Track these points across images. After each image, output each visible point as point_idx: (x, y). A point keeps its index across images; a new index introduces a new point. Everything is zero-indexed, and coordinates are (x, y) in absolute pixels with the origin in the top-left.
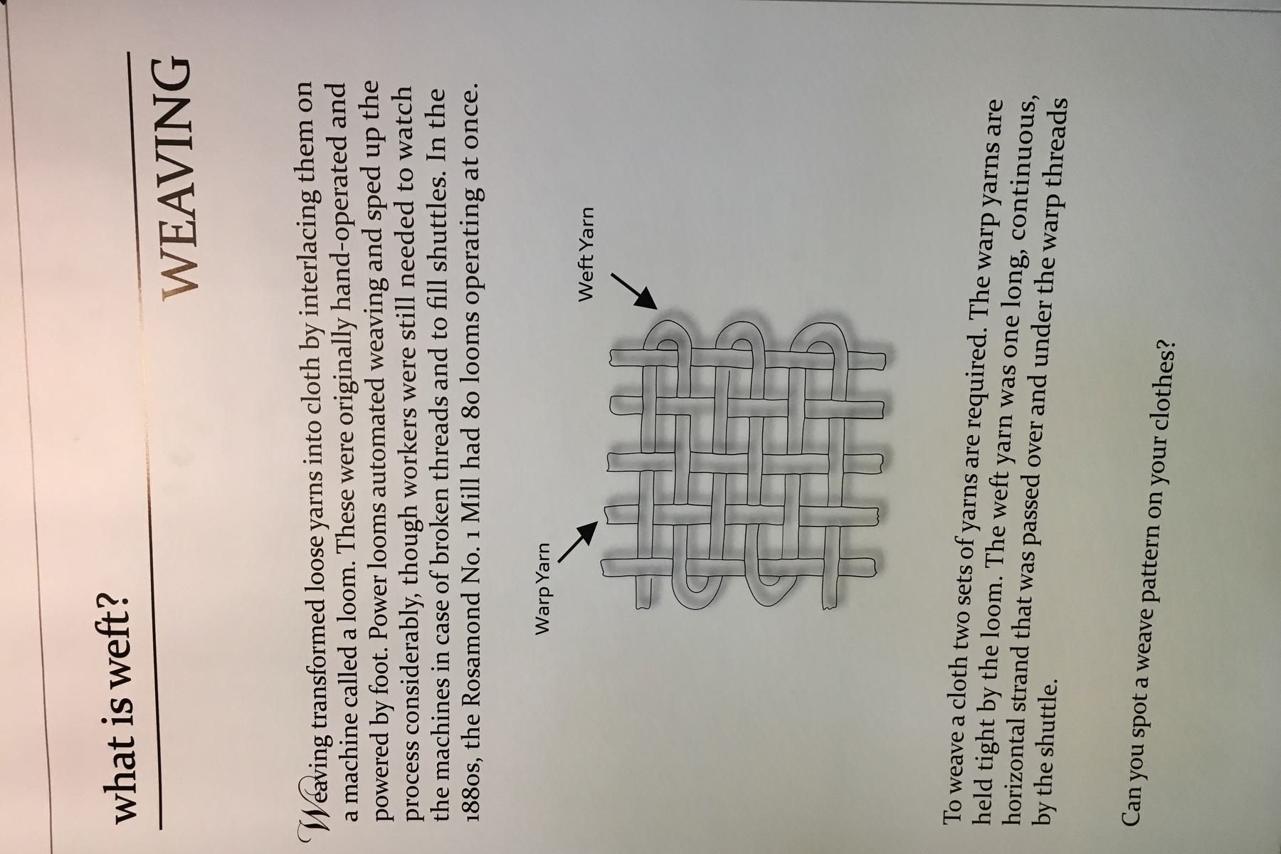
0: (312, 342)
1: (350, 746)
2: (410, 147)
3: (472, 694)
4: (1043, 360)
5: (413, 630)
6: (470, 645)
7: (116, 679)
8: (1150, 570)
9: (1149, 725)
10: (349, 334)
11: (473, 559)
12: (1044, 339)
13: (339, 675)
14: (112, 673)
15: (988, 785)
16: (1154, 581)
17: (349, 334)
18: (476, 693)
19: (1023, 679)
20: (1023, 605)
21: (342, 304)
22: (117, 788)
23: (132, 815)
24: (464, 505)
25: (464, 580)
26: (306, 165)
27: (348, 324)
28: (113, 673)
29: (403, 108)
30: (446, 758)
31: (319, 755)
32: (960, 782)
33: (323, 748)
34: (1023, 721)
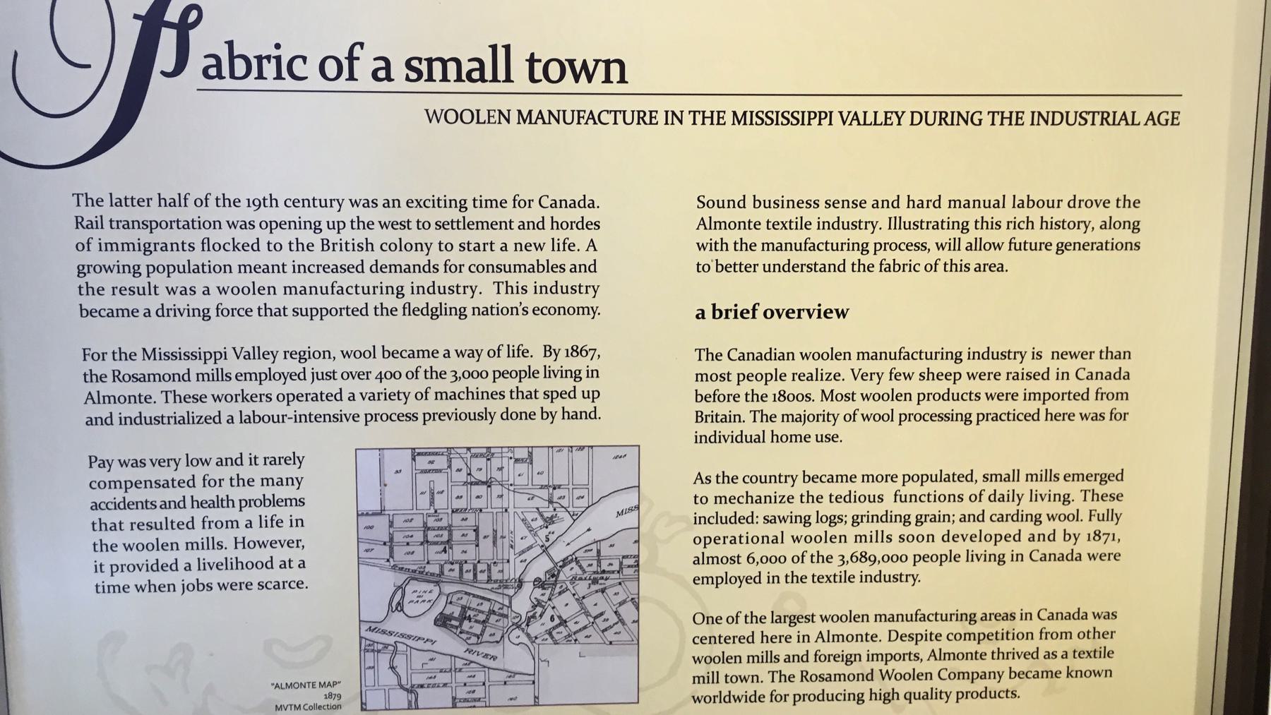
0: (1067, 537)
1: (878, 696)
4: (767, 269)
5: (1025, 205)
8: (129, 202)
9: (151, 232)
12: (781, 269)
14: (585, 62)
16: (121, 205)
19: (126, 226)
20: (191, 224)
21: (566, 415)
24: (154, 349)
26: (810, 498)
27: (492, 418)
28: (585, 63)
30: (999, 500)
31: (390, 289)
33: (997, 559)
34: (102, 228)
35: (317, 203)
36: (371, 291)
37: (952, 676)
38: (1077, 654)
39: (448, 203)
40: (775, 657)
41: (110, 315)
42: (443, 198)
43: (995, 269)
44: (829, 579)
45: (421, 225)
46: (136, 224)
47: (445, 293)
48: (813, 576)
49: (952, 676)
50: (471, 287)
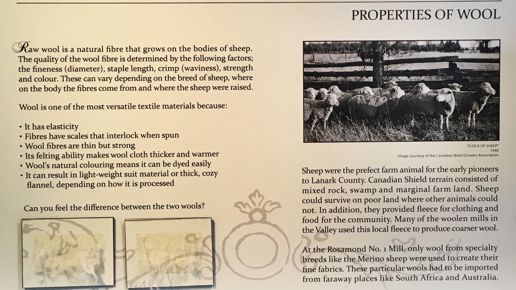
2: (358, 192)
3: (332, 250)
5: (325, 270)
6: (462, 198)
7: (186, 68)
10: (419, 250)
11: (377, 249)
13: (484, 215)
15: (412, 210)
17: (419, 250)
18: (332, 251)
22: (161, 87)
23: (403, 201)
25: (370, 247)
29: (162, 154)
32: (413, 260)
33: (110, 166)
35: (63, 166)
36: (94, 50)
37: (346, 181)
38: (140, 107)
39: (50, 156)
40: (44, 107)
41: (384, 231)
42: (48, 154)
43: (126, 166)
44: (147, 107)
45: (415, 229)
46: (133, 165)
47: (471, 279)
48: (139, 105)
49: (346, 181)
50: (337, 199)
